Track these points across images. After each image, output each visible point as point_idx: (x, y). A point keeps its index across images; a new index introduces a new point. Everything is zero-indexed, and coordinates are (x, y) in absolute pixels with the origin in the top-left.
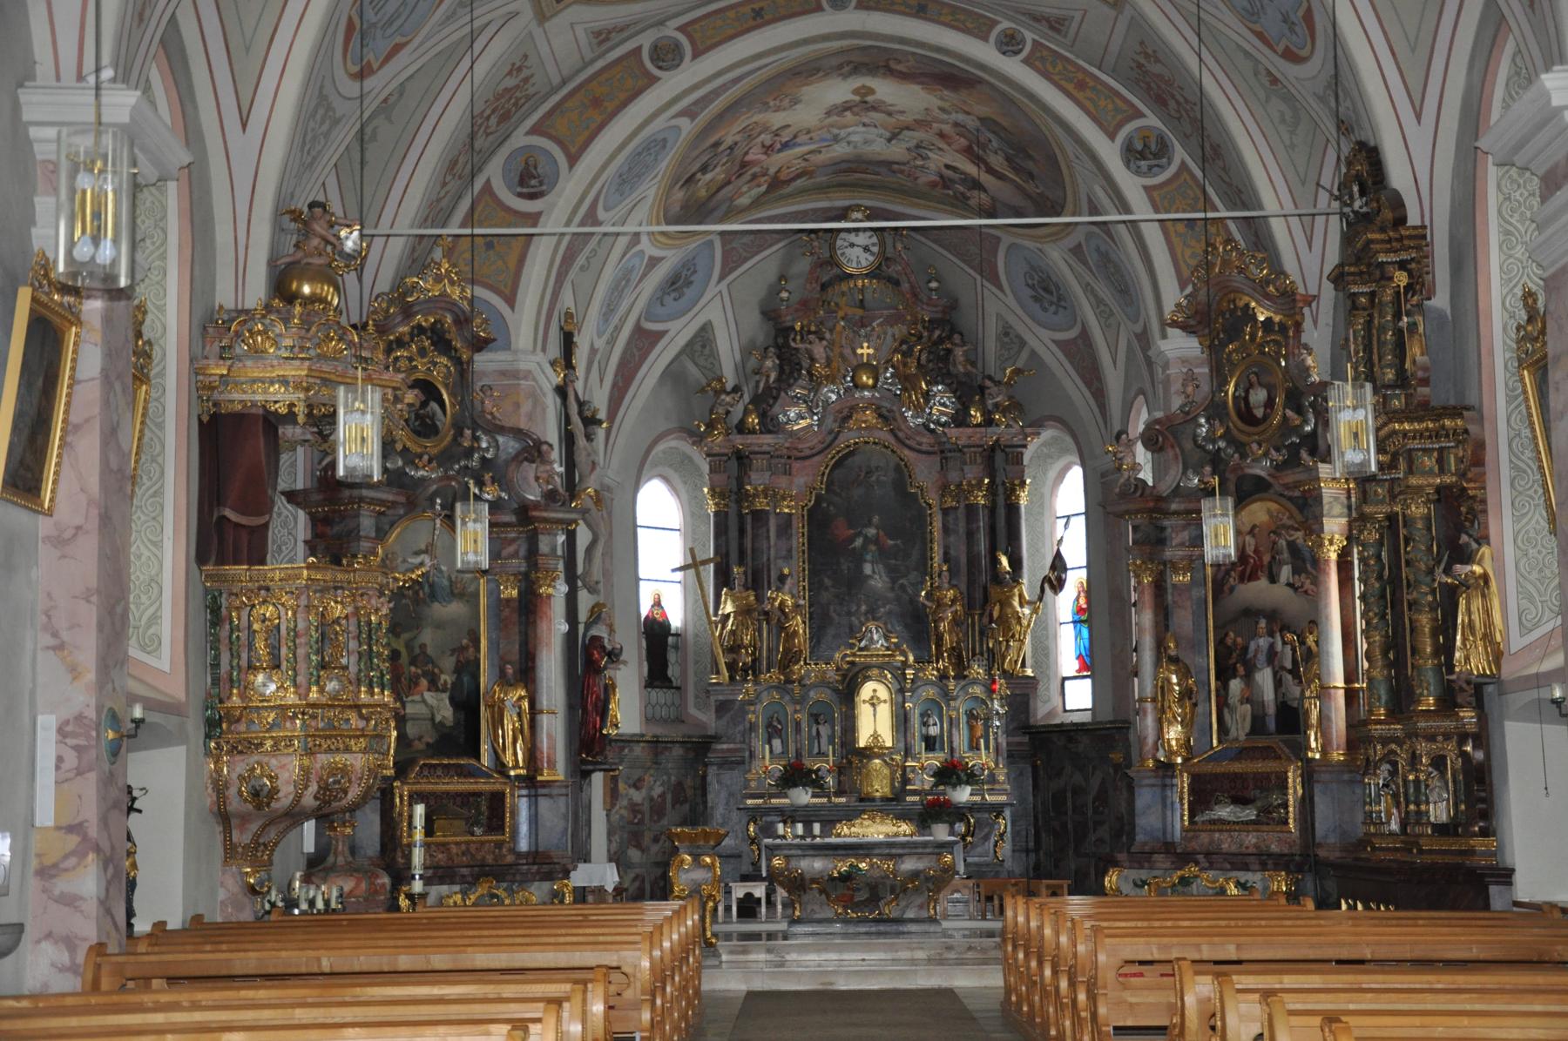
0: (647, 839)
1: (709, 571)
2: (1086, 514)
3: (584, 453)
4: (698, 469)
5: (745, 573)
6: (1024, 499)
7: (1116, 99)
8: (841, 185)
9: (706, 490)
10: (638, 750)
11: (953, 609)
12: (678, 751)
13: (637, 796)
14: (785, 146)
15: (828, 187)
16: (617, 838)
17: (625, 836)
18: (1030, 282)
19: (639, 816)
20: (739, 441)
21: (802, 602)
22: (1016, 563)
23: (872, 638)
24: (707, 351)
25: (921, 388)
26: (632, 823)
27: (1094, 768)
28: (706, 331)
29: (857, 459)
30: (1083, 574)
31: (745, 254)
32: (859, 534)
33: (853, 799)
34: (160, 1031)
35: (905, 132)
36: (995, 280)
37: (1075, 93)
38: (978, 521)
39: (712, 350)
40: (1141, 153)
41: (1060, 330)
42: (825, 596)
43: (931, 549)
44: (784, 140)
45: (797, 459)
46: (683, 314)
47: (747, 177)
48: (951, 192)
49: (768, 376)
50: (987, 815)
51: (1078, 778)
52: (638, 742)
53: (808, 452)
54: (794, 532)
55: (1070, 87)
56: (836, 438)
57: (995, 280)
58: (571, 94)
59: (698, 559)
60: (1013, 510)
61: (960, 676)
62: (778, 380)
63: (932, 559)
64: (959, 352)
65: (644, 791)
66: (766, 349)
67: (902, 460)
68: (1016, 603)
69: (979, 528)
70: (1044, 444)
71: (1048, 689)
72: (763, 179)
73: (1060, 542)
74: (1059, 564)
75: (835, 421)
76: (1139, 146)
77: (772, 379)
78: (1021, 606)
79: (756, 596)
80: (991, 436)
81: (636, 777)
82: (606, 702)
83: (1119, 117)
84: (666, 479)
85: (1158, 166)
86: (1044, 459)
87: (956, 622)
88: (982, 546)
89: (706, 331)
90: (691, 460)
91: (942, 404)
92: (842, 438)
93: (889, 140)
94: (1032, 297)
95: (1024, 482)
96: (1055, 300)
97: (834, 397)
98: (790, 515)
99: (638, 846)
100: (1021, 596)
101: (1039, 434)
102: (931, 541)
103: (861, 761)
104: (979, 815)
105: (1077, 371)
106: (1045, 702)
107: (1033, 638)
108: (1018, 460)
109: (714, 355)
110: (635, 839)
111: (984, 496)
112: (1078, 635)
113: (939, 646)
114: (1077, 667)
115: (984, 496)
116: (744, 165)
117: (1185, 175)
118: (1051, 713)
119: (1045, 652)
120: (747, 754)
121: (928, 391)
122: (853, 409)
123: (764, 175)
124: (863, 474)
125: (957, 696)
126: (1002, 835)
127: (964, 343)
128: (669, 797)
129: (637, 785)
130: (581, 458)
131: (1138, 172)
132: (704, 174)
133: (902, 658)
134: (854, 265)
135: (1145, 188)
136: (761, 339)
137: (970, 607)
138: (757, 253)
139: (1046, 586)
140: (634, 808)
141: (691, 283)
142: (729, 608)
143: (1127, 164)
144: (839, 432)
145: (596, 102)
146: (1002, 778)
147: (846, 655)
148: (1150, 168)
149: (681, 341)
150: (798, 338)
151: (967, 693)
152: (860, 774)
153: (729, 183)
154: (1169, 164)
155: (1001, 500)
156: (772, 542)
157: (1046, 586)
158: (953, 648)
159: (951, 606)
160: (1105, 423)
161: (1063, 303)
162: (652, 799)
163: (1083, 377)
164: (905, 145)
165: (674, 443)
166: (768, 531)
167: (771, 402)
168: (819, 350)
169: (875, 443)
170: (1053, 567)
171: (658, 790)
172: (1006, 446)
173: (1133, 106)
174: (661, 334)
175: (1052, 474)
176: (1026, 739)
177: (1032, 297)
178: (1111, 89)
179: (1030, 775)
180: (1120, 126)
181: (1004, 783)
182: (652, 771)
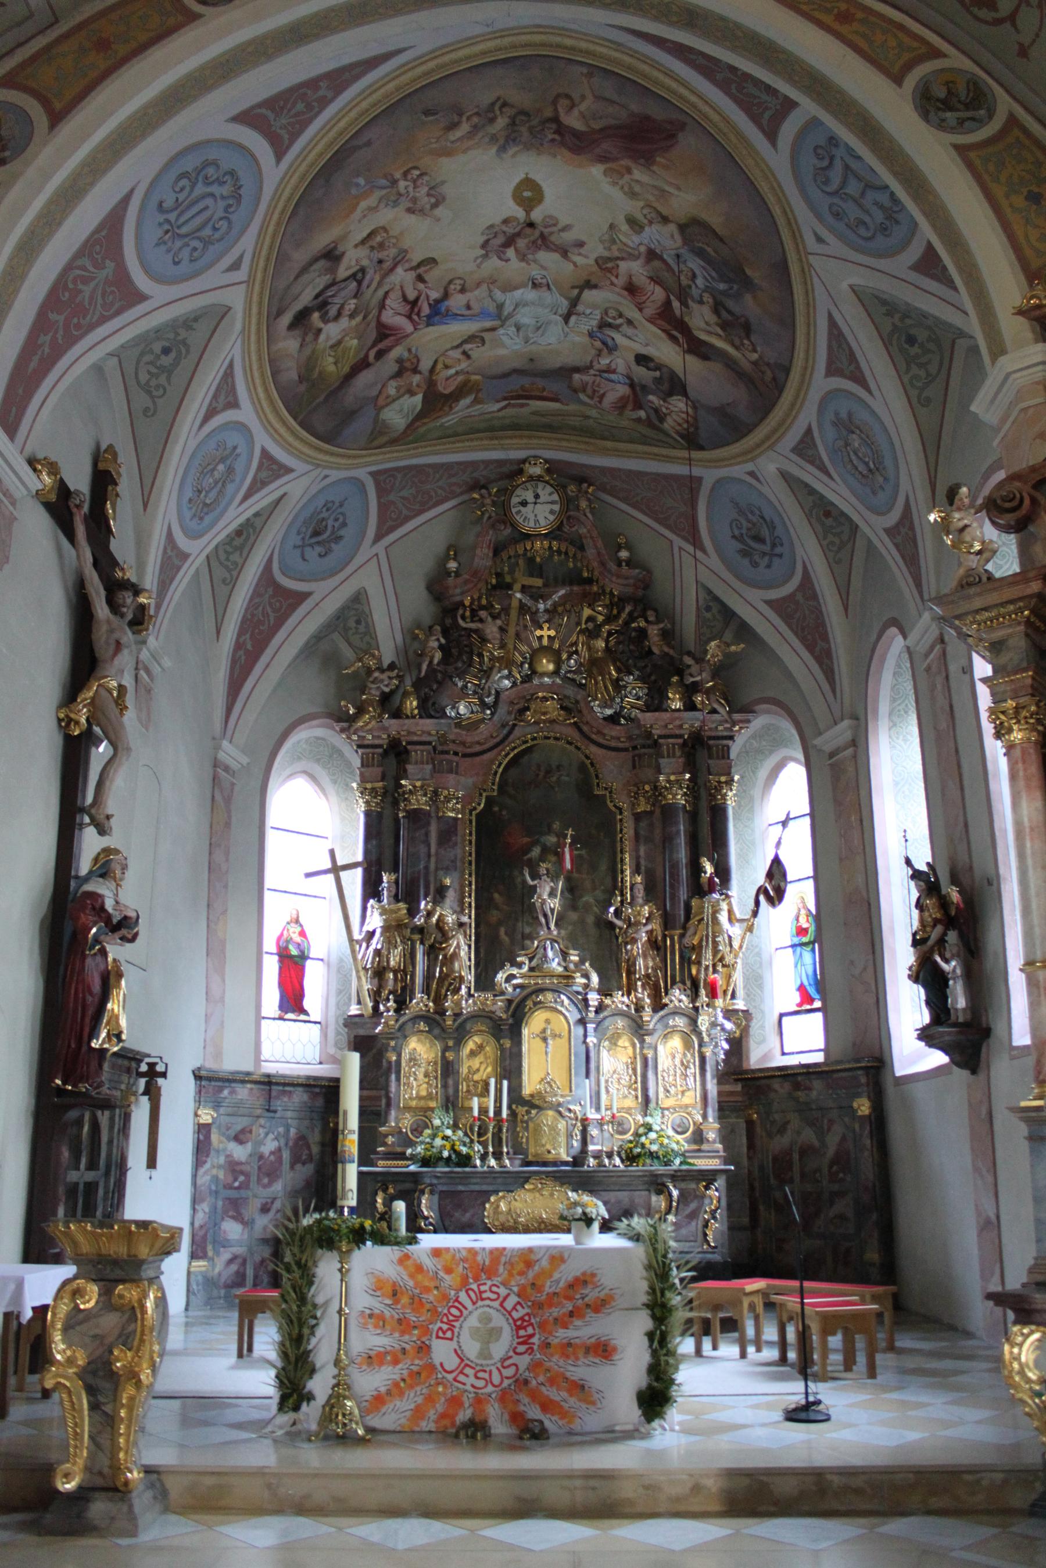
0: (252, 1209)
1: (354, 881)
2: (812, 815)
3: (104, 628)
4: (348, 764)
5: (397, 882)
6: (731, 799)
7: (900, 35)
8: (515, 427)
9: (355, 785)
10: (243, 1092)
11: (649, 927)
12: (299, 1097)
13: (240, 1152)
14: (438, 313)
15: (503, 428)
16: (205, 1207)
17: (220, 1203)
18: (737, 532)
19: (242, 1178)
20: (394, 726)
21: (465, 919)
22: (723, 872)
23: (545, 956)
24: (362, 628)
25: (610, 674)
26: (228, 1187)
27: (831, 1122)
28: (359, 598)
29: (536, 756)
30: (809, 886)
31: (405, 512)
32: (536, 843)
33: (517, 1162)
34: (5, 1359)
35: (588, 295)
36: (695, 540)
37: (836, 26)
38: (677, 823)
39: (367, 626)
40: (944, 102)
41: (778, 587)
42: (494, 916)
43: (622, 860)
44: (434, 295)
45: (465, 755)
46: (333, 573)
47: (388, 365)
48: (642, 414)
49: (432, 658)
50: (693, 1186)
51: (808, 1135)
52: (243, 1082)
53: (477, 748)
54: (459, 839)
55: (828, 19)
56: (510, 733)
57: (695, 540)
58: (59, 41)
59: (340, 863)
60: (719, 814)
61: (658, 1006)
62: (446, 660)
63: (622, 872)
64: (653, 631)
65: (249, 1145)
66: (431, 628)
67: (587, 757)
68: (723, 917)
69: (678, 832)
70: (754, 737)
71: (763, 1027)
72: (416, 379)
73: (778, 844)
74: (776, 871)
75: (509, 713)
76: (941, 93)
77: (436, 661)
78: (730, 920)
79: (409, 910)
80: (692, 721)
81: (239, 1128)
82: (105, 997)
83: (906, 56)
84: (313, 778)
85: (973, 119)
86: (755, 754)
87: (654, 944)
88: (682, 854)
89: (359, 598)
90: (340, 753)
91: (634, 692)
92: (517, 732)
93: (566, 318)
94: (740, 551)
95: (733, 780)
96: (767, 548)
97: (507, 683)
98: (456, 819)
99: (238, 1218)
100: (730, 912)
101: (748, 721)
102: (622, 852)
103: (528, 1112)
104: (683, 1185)
105: (796, 634)
106: (759, 1043)
107: (745, 964)
108: (725, 753)
109: (370, 632)
110: (235, 1208)
111: (685, 794)
112: (799, 961)
113: (631, 972)
114: (798, 1000)
115: (685, 794)
116: (384, 332)
117: (1016, 132)
118: (766, 1057)
119: (756, 981)
120: (384, 1101)
121: (618, 680)
122: (533, 698)
123: (415, 371)
124: (542, 774)
125: (654, 1030)
126: (713, 1213)
127: (658, 621)
128: (286, 1155)
129: (239, 1138)
130: (101, 636)
131: (941, 126)
132: (325, 319)
133: (584, 981)
134: (532, 524)
135: (956, 147)
136: (427, 621)
137: (668, 922)
138: (421, 512)
139: (762, 898)
140: (233, 1167)
141: (341, 537)
142: (375, 921)
143: (925, 115)
144: (514, 725)
145: (103, 45)
146: (711, 1136)
147: (512, 977)
148: (961, 122)
149: (331, 606)
150: (468, 614)
151: (667, 1026)
152: (527, 1129)
153: (362, 365)
154: (991, 116)
155: (704, 804)
156: (433, 851)
157: (762, 898)
158: (647, 976)
159: (645, 925)
160: (834, 691)
161: (778, 550)
162: (261, 1157)
163: (803, 640)
164: (585, 328)
165: (320, 732)
166: (427, 834)
167: (435, 687)
168: (491, 629)
169: (556, 739)
170: (770, 875)
171: (269, 1146)
172: (711, 738)
173: (928, 43)
174: (303, 596)
175: (763, 773)
176: (738, 1087)
177: (740, 551)
178: (890, 21)
179: (744, 1132)
180: (908, 67)
181: (714, 1142)
182: (262, 1121)
